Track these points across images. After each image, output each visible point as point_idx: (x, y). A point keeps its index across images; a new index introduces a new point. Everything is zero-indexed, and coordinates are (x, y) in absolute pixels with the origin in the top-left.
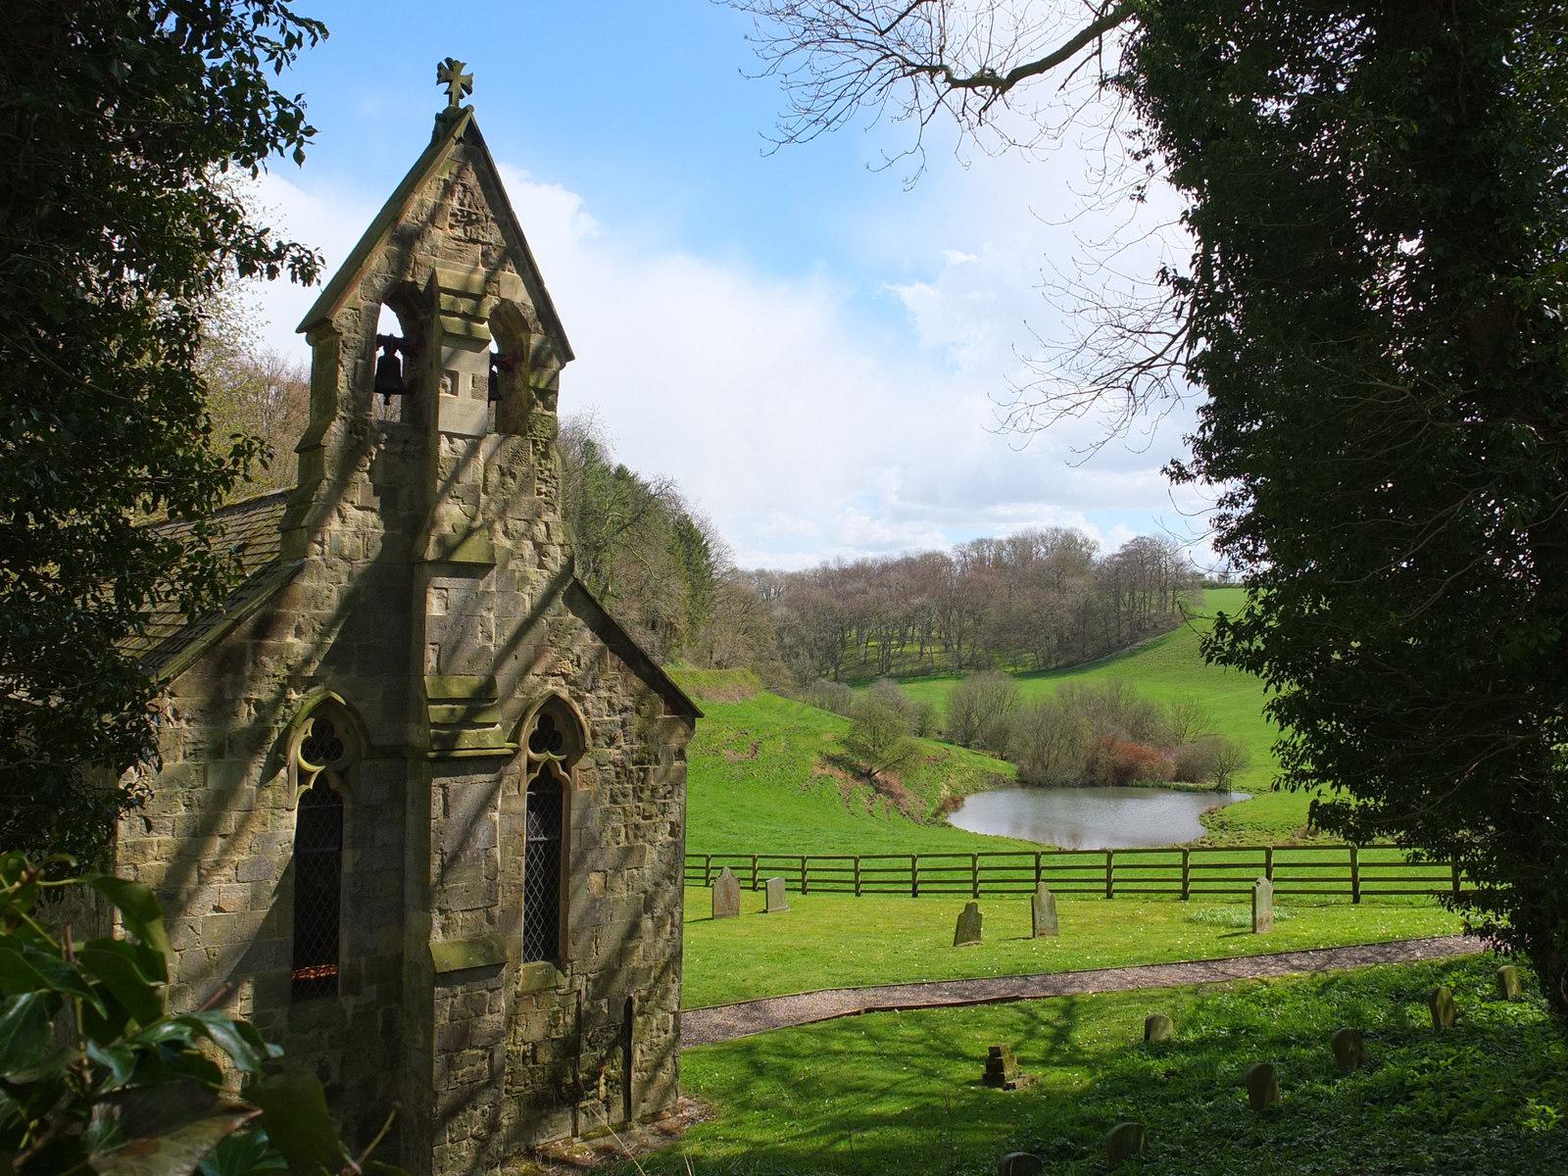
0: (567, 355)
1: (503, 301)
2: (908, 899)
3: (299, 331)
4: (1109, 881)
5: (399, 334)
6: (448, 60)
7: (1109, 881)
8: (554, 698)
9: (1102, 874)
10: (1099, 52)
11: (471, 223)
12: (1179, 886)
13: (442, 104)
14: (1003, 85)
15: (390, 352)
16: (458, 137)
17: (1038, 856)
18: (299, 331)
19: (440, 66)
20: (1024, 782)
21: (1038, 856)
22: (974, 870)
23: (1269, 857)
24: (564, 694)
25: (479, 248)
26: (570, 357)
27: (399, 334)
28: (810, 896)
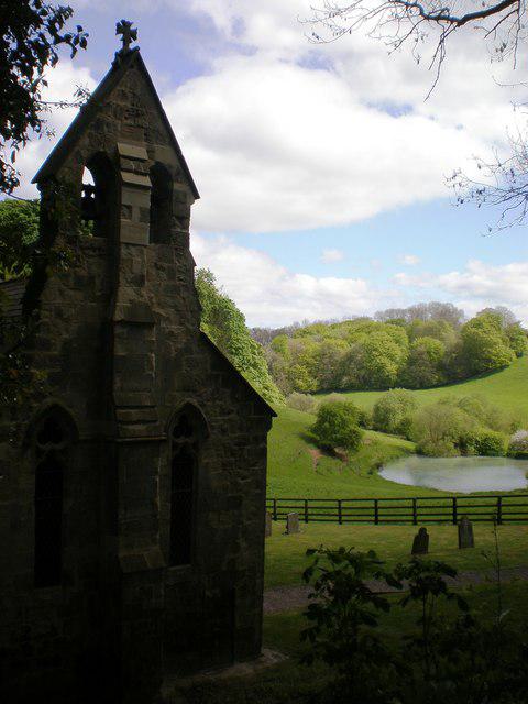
0: (197, 196)
1: (158, 163)
2: (336, 524)
3: (33, 182)
4: (414, 515)
5: (93, 184)
6: (123, 22)
7: (340, 515)
8: (189, 406)
9: (336, 512)
10: (518, 10)
11: (138, 115)
12: (411, 518)
13: (119, 46)
14: (461, 22)
15: (88, 194)
16: (128, 65)
17: (376, 501)
18: (33, 182)
19: (118, 25)
20: (420, 452)
21: (376, 501)
22: (414, 507)
23: (454, 501)
24: (195, 402)
25: (143, 131)
26: (198, 197)
27: (93, 184)
28: (345, 525)
